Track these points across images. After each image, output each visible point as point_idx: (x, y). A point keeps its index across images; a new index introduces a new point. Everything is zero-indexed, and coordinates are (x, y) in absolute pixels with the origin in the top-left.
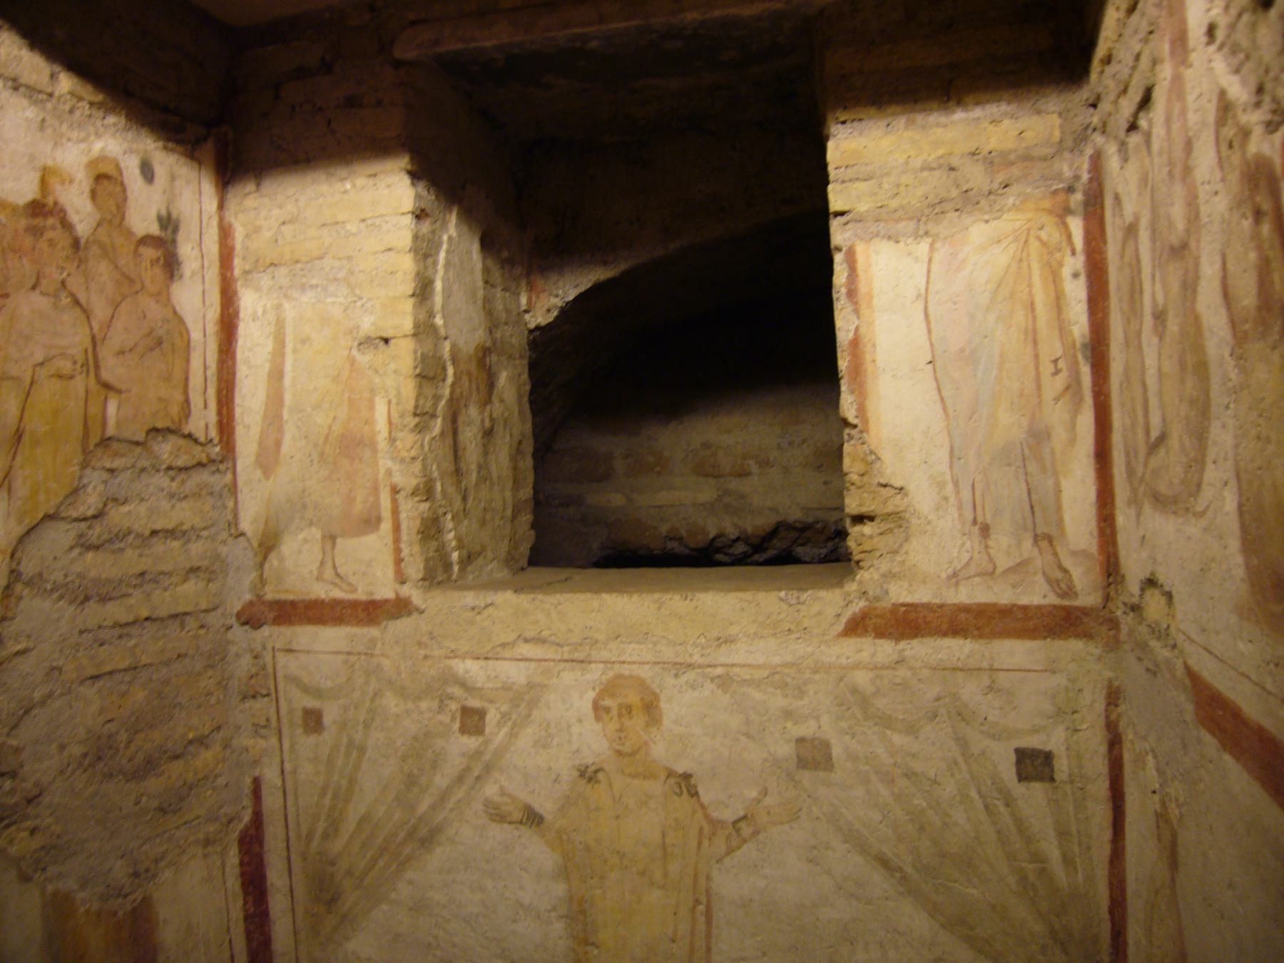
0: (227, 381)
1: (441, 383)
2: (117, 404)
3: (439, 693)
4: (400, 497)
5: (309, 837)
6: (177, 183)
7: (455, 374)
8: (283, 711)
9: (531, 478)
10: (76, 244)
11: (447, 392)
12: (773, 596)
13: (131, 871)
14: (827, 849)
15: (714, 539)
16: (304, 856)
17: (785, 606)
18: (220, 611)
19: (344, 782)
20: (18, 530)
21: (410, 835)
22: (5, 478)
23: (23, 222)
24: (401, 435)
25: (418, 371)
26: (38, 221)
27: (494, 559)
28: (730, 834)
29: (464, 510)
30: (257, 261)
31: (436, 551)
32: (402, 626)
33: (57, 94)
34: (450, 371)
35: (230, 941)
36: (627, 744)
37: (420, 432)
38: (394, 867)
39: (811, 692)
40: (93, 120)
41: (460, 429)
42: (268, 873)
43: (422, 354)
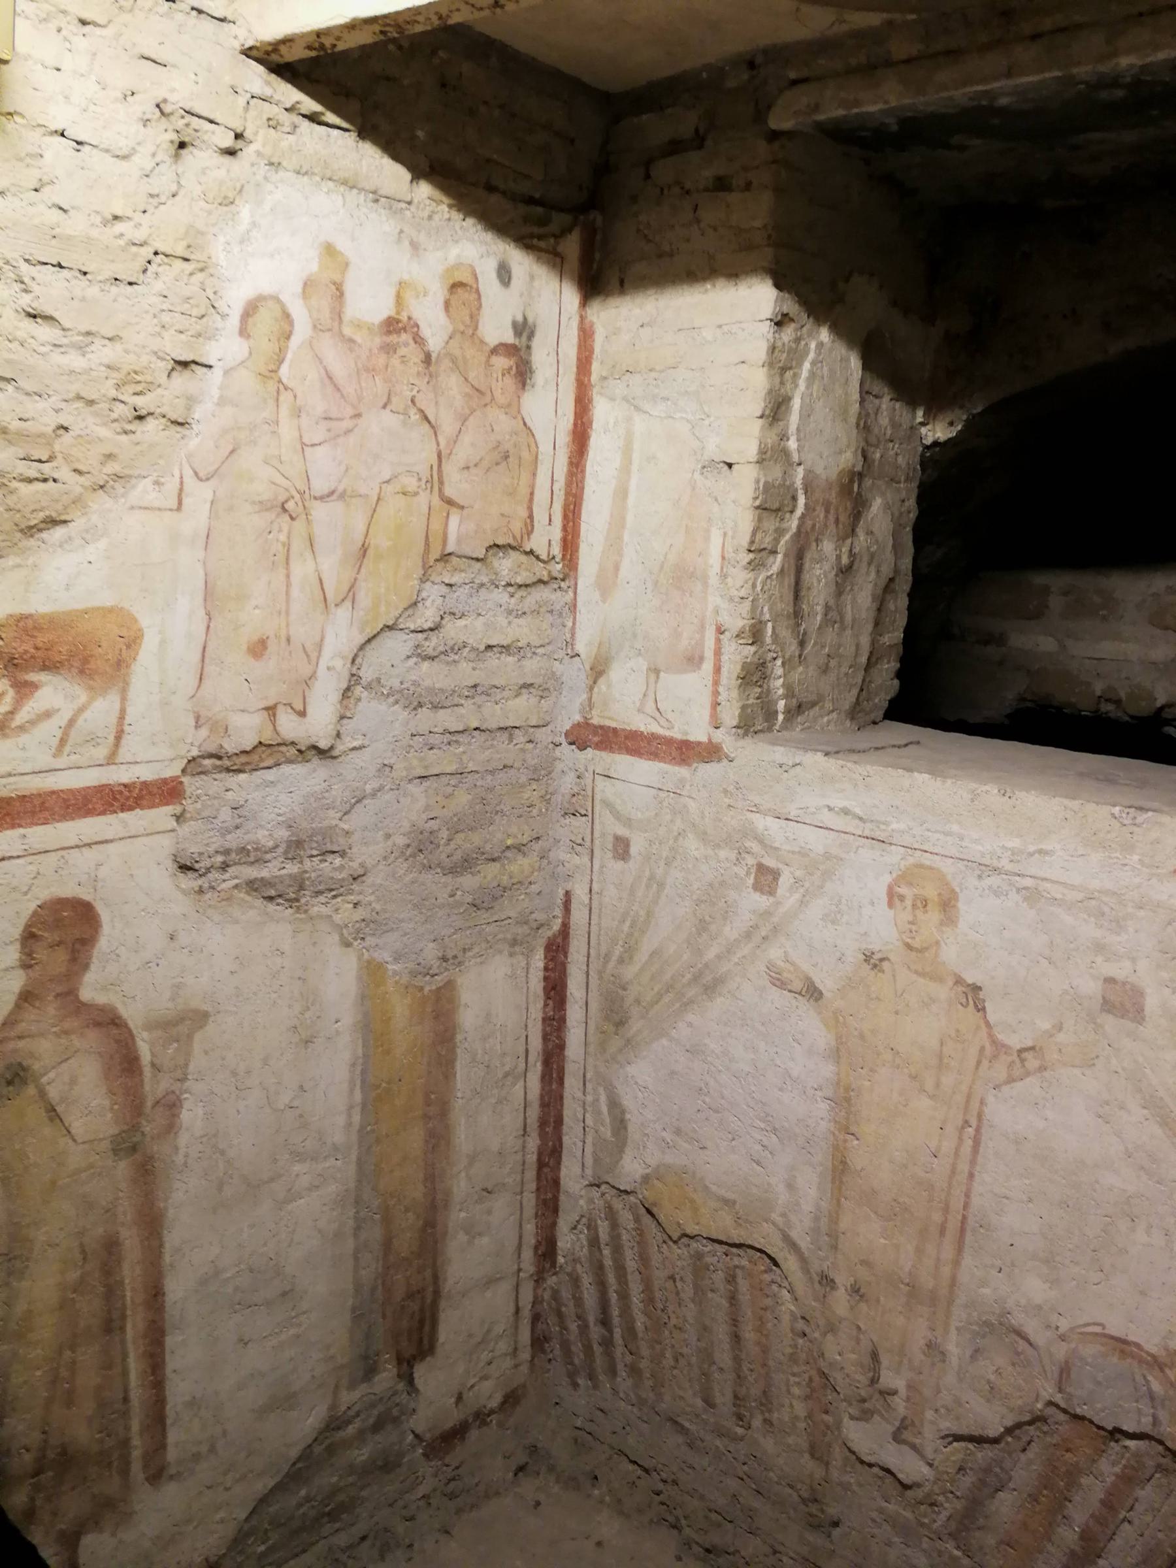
0: (575, 496)
1: (788, 515)
2: (458, 521)
3: (737, 845)
4: (725, 638)
5: (607, 958)
6: (536, 284)
7: (806, 504)
8: (597, 834)
9: (902, 620)
10: (427, 359)
11: (794, 524)
12: (1105, 810)
13: (440, 955)
14: (1121, 1108)
15: (1162, 708)
16: (600, 973)
17: (1117, 824)
18: (549, 728)
19: (642, 913)
20: (361, 639)
21: (696, 978)
22: (350, 591)
23: (378, 340)
24: (732, 571)
25: (757, 503)
26: (393, 338)
27: (833, 711)
28: (1013, 1062)
29: (800, 656)
30: (614, 367)
31: (758, 698)
32: (709, 771)
33: (416, 201)
34: (802, 500)
35: (527, 1037)
36: (917, 939)
37: (753, 570)
38: (678, 1005)
39: (1131, 930)
40: (451, 223)
41: (807, 566)
42: (569, 982)
43: (766, 483)
